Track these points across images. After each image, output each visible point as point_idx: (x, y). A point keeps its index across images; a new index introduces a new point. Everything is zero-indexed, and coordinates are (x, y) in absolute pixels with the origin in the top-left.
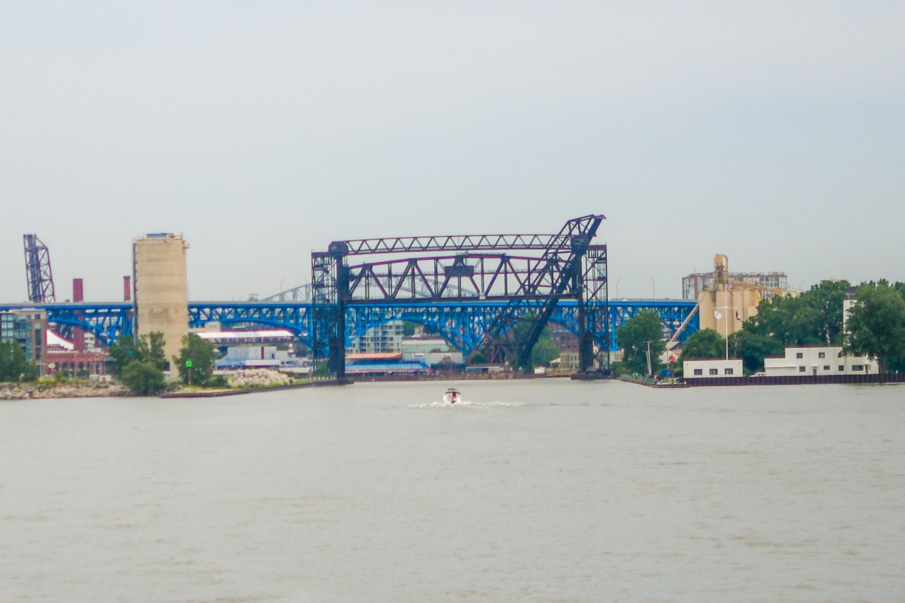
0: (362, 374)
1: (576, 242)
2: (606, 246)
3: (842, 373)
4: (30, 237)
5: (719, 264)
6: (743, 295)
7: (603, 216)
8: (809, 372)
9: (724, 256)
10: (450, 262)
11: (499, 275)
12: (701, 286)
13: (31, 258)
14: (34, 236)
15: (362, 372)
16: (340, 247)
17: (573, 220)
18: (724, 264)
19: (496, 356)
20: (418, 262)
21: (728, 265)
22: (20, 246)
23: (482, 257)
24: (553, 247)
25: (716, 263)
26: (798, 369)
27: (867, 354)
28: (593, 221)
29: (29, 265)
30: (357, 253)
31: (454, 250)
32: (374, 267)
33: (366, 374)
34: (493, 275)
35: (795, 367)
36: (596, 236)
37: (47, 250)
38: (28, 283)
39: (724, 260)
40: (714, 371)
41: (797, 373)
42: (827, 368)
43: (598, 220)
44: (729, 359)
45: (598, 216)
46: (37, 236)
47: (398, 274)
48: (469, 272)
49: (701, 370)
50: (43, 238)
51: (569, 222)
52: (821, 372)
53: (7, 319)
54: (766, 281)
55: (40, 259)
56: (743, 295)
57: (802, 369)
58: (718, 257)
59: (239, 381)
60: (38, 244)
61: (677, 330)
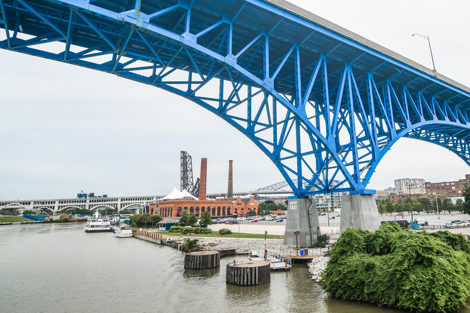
4: (184, 152)
11: (246, 97)
13: (183, 161)
19: (339, 84)
22: (179, 155)
24: (363, 146)
34: (252, 94)
37: (191, 157)
38: (181, 186)
47: (57, 226)
50: (189, 153)
55: (187, 161)
60: (187, 155)
61: (180, 31)
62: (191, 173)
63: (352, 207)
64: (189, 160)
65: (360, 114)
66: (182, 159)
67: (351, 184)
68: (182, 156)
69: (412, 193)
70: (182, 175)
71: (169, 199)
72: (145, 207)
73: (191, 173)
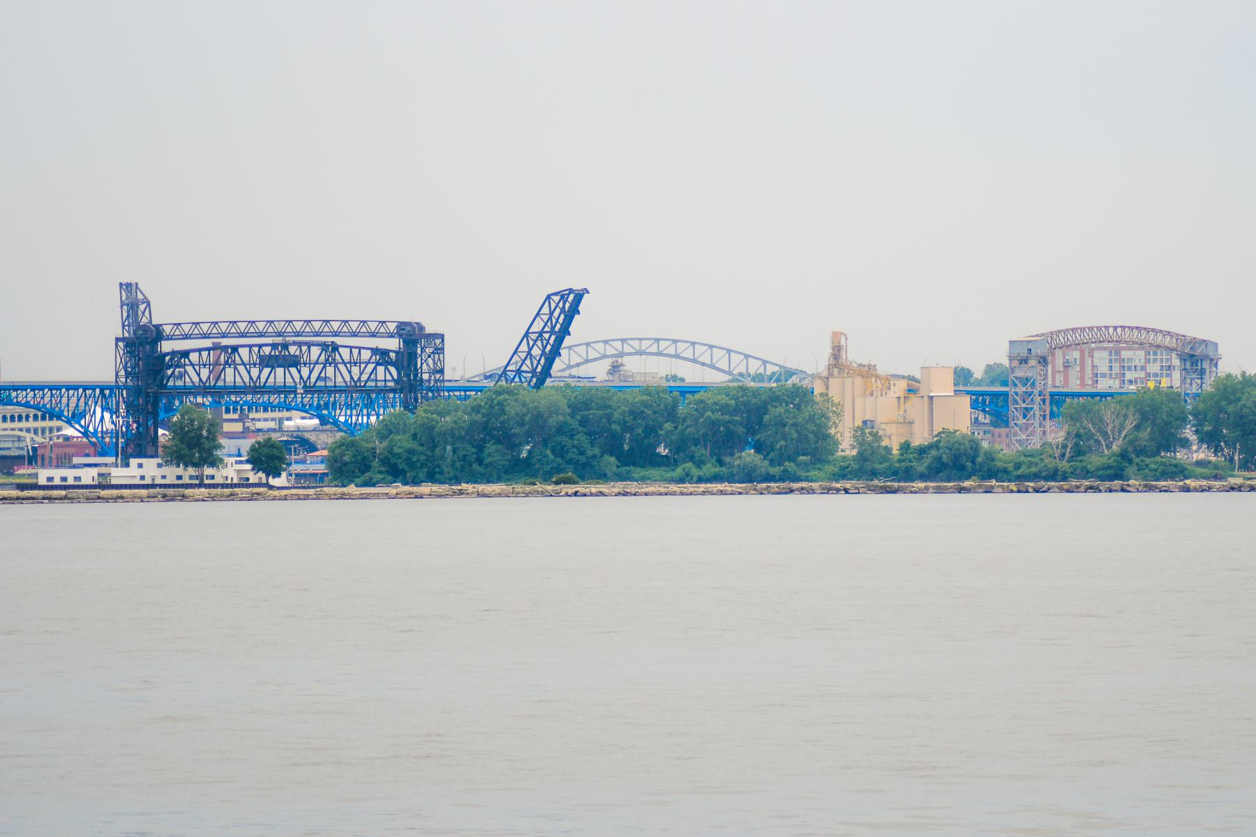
0: (317, 474)
1: (402, 330)
2: (443, 335)
3: (180, 482)
4: (129, 285)
5: (836, 344)
6: (853, 383)
7: (586, 289)
8: (148, 481)
9: (841, 334)
10: (267, 350)
12: (1061, 361)
14: (134, 288)
15: (316, 472)
16: (147, 331)
17: (556, 294)
18: (843, 343)
20: (239, 349)
21: (848, 345)
23: (309, 345)
25: (833, 342)
26: (139, 478)
27: (181, 465)
28: (571, 297)
29: (126, 323)
30: (170, 338)
31: (273, 336)
32: (191, 354)
33: (321, 474)
35: (135, 476)
36: (579, 313)
37: (149, 304)
39: (843, 337)
40: (64, 479)
41: (138, 481)
42: (164, 477)
43: (579, 297)
44: (121, 467)
45: (578, 290)
46: (139, 285)
48: (294, 362)
49: (53, 478)
51: (549, 297)
52: (159, 481)
53: (326, 384)
54: (1166, 359)
56: (853, 383)
57: (143, 478)
58: (836, 335)
59: (410, 476)
60: (140, 296)
62: (147, 313)
63: (574, 310)
64: (143, 313)
65: (63, 418)
66: (125, 307)
67: (318, 345)
68: (124, 298)
69: (298, 396)
70: (125, 314)
71: (74, 437)
72: (30, 451)
73: (147, 313)
